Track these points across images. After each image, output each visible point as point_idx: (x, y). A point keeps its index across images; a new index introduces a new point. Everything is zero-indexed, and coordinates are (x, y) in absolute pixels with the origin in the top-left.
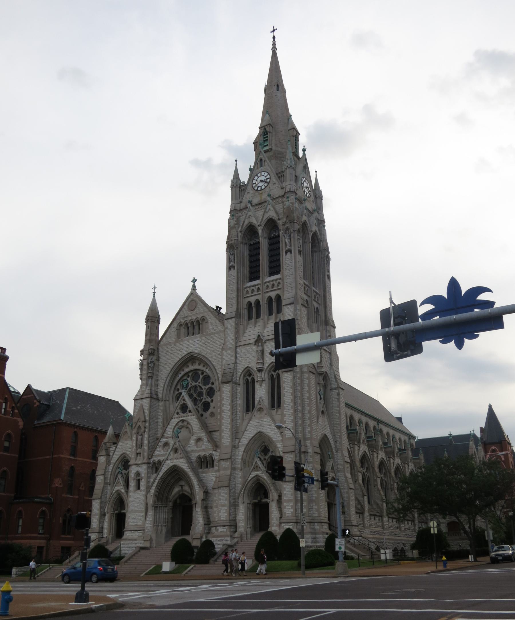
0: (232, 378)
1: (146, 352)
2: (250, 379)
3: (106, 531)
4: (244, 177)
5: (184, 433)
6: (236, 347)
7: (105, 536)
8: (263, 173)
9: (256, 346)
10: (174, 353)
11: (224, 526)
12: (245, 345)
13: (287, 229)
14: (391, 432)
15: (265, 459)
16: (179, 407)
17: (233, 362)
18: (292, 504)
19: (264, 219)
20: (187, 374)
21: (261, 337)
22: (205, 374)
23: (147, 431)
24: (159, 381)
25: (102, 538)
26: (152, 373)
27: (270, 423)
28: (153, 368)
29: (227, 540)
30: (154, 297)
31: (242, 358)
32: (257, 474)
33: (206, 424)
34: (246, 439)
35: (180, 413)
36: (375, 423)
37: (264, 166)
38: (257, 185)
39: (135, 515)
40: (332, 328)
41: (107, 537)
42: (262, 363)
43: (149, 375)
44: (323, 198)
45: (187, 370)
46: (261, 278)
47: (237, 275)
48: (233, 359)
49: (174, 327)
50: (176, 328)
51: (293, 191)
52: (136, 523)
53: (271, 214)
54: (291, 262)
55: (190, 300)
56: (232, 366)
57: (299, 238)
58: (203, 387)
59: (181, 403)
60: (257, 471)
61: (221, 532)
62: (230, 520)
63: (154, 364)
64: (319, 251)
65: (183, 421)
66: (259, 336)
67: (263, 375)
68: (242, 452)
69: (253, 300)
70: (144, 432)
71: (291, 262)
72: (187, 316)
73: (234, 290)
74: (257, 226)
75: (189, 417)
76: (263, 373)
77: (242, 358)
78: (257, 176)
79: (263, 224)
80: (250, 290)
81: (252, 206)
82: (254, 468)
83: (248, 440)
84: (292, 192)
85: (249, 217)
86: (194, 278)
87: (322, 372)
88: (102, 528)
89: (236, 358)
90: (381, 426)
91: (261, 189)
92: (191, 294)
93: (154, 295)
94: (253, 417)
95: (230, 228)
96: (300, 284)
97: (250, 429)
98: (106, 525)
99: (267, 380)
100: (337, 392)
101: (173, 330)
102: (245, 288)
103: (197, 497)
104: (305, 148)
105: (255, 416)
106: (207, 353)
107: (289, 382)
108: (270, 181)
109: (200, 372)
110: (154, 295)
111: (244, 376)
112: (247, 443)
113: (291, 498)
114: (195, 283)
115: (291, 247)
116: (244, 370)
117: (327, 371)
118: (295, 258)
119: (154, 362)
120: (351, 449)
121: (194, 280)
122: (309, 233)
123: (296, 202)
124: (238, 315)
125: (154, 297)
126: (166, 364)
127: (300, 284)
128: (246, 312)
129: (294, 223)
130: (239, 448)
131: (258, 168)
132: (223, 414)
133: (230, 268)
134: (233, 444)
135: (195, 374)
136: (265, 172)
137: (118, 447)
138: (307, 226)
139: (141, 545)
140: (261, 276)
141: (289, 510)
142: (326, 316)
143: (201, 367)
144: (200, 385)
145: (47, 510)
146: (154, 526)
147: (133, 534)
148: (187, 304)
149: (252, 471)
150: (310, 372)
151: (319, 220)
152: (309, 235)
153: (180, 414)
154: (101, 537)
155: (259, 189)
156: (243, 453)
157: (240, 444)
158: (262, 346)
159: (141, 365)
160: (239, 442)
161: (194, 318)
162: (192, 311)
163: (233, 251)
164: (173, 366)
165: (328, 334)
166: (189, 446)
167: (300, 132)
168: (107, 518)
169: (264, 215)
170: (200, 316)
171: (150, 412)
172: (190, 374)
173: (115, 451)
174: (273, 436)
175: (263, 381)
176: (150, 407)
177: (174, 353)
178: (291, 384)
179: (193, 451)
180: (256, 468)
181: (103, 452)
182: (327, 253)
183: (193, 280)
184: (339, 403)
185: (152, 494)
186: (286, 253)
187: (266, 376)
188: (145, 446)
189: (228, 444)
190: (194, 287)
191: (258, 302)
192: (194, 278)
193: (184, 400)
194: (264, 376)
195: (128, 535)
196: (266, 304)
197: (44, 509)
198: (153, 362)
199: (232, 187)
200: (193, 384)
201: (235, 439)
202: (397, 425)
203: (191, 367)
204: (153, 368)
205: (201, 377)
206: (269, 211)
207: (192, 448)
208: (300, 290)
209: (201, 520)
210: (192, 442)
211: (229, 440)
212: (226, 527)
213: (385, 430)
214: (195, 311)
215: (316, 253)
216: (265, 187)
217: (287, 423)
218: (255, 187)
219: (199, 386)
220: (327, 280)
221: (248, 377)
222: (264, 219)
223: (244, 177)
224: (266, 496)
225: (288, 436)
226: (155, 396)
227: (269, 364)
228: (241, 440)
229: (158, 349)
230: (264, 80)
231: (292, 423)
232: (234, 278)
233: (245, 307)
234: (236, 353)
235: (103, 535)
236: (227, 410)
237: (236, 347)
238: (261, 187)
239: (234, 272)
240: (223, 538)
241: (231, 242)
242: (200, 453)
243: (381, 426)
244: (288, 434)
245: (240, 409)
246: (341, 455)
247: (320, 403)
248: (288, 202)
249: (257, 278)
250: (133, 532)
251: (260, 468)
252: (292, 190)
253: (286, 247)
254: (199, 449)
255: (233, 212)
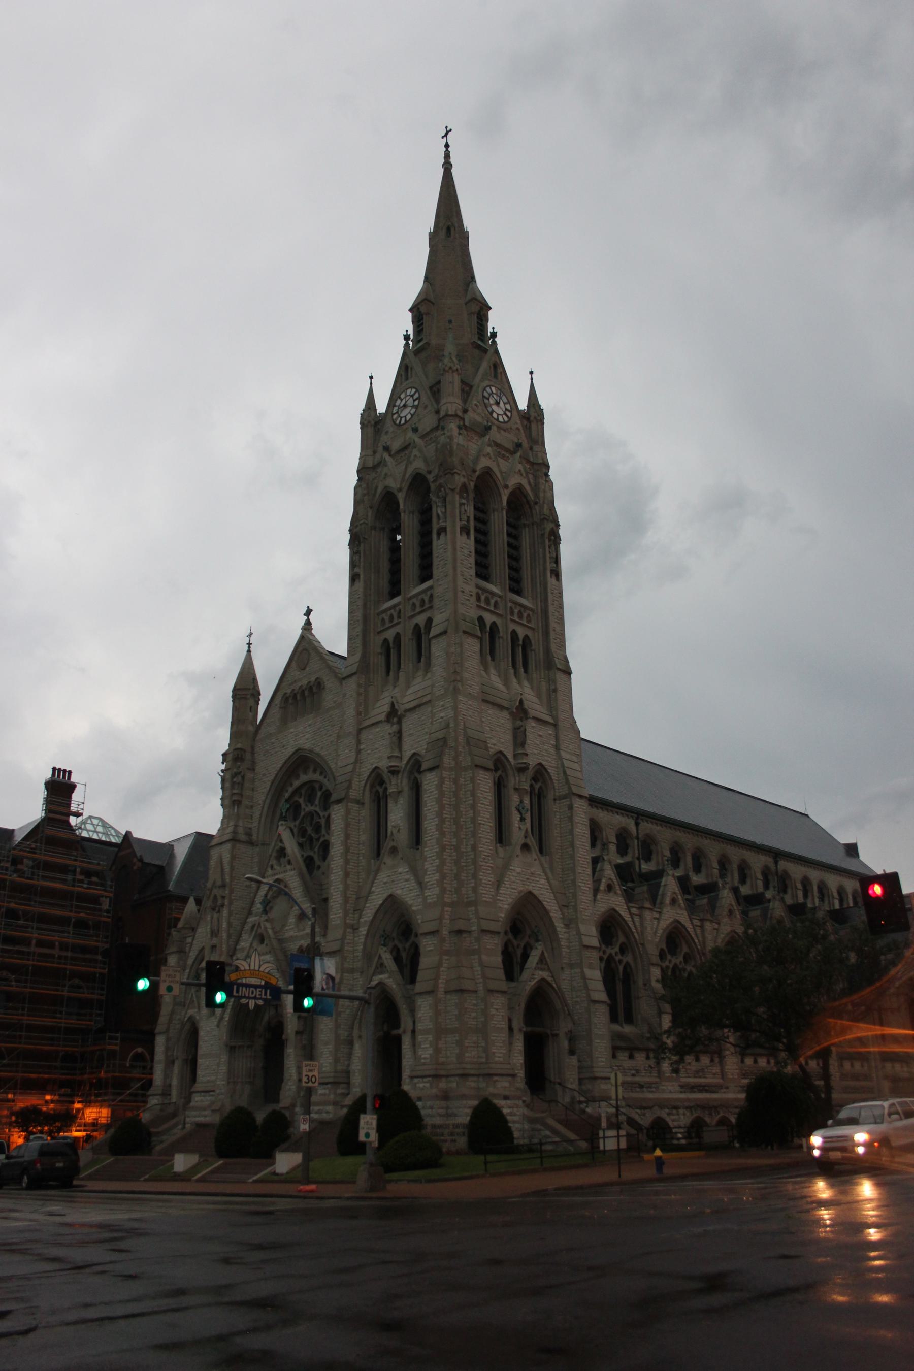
0: (348, 792)
1: (230, 757)
2: (381, 790)
3: (174, 1092)
4: (381, 407)
5: (280, 905)
6: (360, 731)
7: (174, 1100)
8: (409, 391)
9: (390, 725)
10: (276, 752)
11: (327, 1083)
12: (373, 724)
13: (440, 486)
14: (815, 875)
15: (405, 949)
16: (274, 854)
17: (352, 760)
18: (430, 1038)
19: (407, 476)
20: (297, 791)
21: (396, 707)
22: (324, 789)
23: (226, 903)
24: (254, 808)
25: (169, 1104)
26: (241, 795)
27: (407, 877)
28: (241, 785)
29: (327, 1112)
30: (249, 651)
31: (368, 752)
32: (381, 979)
33: (322, 885)
34: (371, 909)
35: (275, 867)
36: (769, 861)
37: (412, 376)
38: (399, 416)
39: (207, 1063)
40: (560, 677)
41: (175, 1103)
42: (397, 757)
43: (235, 798)
44: (545, 421)
45: (296, 783)
46: (402, 593)
47: (547, 606)
48: (353, 754)
49: (276, 705)
50: (278, 706)
51: (453, 413)
52: (209, 1078)
53: (418, 465)
54: (445, 552)
55: (300, 649)
56: (350, 768)
57: (464, 501)
58: (321, 814)
59: (277, 848)
60: (381, 973)
61: (321, 1095)
62: (335, 1072)
63: (243, 777)
64: (533, 524)
65: (278, 881)
66: (393, 704)
67: (399, 781)
68: (364, 937)
69: (390, 635)
70: (223, 906)
71: (445, 552)
72: (295, 681)
73: (358, 621)
74: (395, 492)
75: (288, 874)
76: (400, 776)
77: (368, 752)
78: (400, 398)
79: (405, 486)
80: (386, 617)
81: (390, 456)
82: (377, 968)
83: (374, 911)
84: (452, 416)
85: (385, 478)
86: (308, 607)
87: (523, 765)
88: (170, 1086)
89: (359, 752)
90: (783, 865)
91: (406, 422)
92: (302, 637)
93: (249, 647)
94: (383, 866)
95: (357, 503)
96: (463, 592)
97: (378, 890)
98: (175, 1082)
99: (406, 789)
100: (568, 803)
101: (275, 710)
102: (378, 614)
103: (290, 1027)
104: (495, 331)
105: (385, 863)
106: (322, 748)
107: (433, 791)
108: (419, 403)
109: (317, 786)
110: (249, 647)
111: (372, 786)
112: (371, 918)
113: (429, 1027)
114: (310, 617)
115: (446, 522)
116: (371, 773)
117: (544, 763)
118: (454, 543)
119: (242, 774)
120: (632, 918)
121: (308, 612)
122: (501, 490)
123: (460, 434)
124: (364, 667)
125: (249, 651)
126: (264, 775)
127: (463, 592)
128: (382, 660)
129: (453, 474)
130: (360, 929)
131: (401, 384)
132: (332, 863)
133: (354, 578)
134: (348, 921)
135: (310, 789)
136: (412, 388)
137: (196, 936)
138: (494, 477)
139: (201, 1119)
140: (402, 590)
141: (426, 1052)
142: (548, 651)
143: (317, 777)
144: (317, 809)
145: (145, 1051)
146: (229, 1083)
147: (202, 1098)
148: (295, 658)
149: (374, 974)
150: (477, 766)
151: (532, 464)
152: (500, 495)
153: (275, 869)
154: (168, 1102)
155: (403, 422)
156: (366, 939)
157: (362, 920)
158: (399, 722)
159: (223, 780)
160: (360, 917)
161: (305, 682)
162: (303, 670)
163: (359, 545)
164: (272, 778)
165: (552, 687)
166: (287, 928)
167: (490, 304)
168: (176, 1069)
169: (406, 468)
170: (313, 679)
171: (232, 868)
172: (303, 792)
173: (191, 944)
174: (412, 902)
175: (400, 792)
176: (233, 857)
177: (276, 752)
178: (436, 794)
179: (292, 937)
180: (381, 967)
181: (173, 949)
182: (551, 525)
183: (307, 611)
184: (572, 825)
185: (226, 1023)
186: (439, 534)
187: (405, 782)
188: (223, 932)
189: (339, 922)
190: (308, 623)
191: (398, 637)
192: (308, 607)
193: (281, 841)
194: (401, 783)
195: (197, 1099)
196: (412, 639)
197: (140, 1050)
198: (240, 773)
199: (364, 425)
200: (307, 810)
201: (355, 911)
202: (849, 864)
203: (304, 778)
204: (242, 784)
205: (319, 794)
206: (414, 460)
207: (291, 933)
208: (463, 604)
209: (294, 1071)
210: (290, 920)
211: (341, 914)
212: (329, 1086)
213: (796, 872)
214: (307, 669)
215: (527, 529)
216: (412, 416)
217: (429, 875)
218: (396, 419)
219: (316, 812)
220: (551, 581)
221: (378, 788)
222: (407, 476)
223: (381, 407)
224: (397, 1025)
225: (430, 901)
226: (243, 837)
227: (408, 758)
228: (364, 913)
229: (253, 748)
230: (428, 222)
231: (437, 872)
232: (359, 598)
233: (379, 650)
234: (359, 742)
235: (170, 1099)
236: (339, 855)
237: (360, 731)
238: (405, 417)
239: (360, 585)
240: (321, 1108)
241: (355, 530)
242: (302, 942)
243: (783, 865)
244: (430, 896)
245: (363, 851)
246: (575, 933)
247: (520, 828)
248: (443, 436)
249: (398, 593)
250: (203, 1094)
251: (386, 967)
252: (450, 413)
253: (438, 523)
254: (301, 933)
255: (362, 471)
